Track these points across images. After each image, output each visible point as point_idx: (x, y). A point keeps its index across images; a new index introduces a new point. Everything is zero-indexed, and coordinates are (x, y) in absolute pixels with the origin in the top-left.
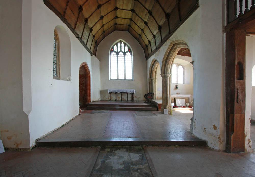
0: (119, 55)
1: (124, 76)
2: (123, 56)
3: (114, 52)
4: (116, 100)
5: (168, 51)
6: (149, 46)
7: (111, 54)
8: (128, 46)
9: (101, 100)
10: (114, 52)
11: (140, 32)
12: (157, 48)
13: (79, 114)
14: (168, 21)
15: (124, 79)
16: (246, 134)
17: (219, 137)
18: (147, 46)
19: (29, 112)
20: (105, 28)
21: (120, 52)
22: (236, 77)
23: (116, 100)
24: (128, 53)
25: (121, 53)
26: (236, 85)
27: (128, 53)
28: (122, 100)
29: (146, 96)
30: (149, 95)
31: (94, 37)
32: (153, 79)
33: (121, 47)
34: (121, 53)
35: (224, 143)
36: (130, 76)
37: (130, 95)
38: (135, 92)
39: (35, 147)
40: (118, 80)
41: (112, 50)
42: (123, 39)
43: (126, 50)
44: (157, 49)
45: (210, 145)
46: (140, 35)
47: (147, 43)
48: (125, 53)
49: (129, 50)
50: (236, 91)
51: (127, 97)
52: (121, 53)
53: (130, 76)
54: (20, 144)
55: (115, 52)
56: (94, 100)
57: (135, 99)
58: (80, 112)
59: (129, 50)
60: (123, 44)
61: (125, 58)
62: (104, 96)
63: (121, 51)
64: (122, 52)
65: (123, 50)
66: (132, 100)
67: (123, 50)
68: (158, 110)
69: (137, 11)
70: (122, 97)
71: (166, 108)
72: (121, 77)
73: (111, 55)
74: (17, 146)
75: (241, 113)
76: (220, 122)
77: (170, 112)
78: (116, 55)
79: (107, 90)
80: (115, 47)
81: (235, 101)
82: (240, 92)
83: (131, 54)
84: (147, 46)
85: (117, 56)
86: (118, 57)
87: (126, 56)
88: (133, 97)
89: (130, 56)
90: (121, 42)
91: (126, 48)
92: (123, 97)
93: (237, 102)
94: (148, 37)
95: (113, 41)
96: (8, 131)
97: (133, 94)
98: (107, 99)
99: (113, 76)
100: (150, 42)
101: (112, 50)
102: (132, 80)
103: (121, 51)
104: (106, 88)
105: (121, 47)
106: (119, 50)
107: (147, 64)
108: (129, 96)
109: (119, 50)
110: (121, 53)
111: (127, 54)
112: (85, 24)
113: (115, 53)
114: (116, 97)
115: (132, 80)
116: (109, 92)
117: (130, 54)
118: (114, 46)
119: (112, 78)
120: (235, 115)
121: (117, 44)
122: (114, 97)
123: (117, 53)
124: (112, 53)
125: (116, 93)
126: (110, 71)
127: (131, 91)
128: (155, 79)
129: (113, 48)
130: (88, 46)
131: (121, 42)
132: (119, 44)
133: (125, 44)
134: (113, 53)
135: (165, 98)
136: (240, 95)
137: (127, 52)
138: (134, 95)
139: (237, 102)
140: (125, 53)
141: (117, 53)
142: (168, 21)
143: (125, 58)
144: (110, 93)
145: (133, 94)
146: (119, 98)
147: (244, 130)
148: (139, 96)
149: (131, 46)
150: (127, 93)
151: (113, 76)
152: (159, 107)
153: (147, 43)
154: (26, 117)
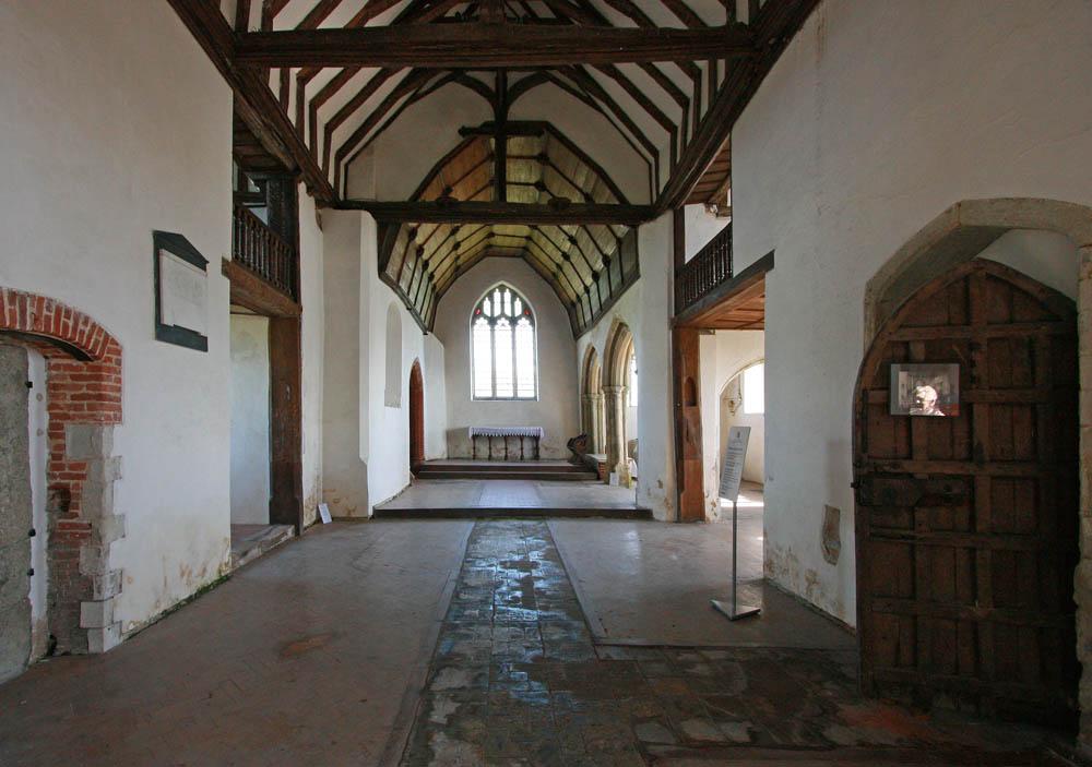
0: (496, 327)
1: (511, 387)
2: (509, 328)
3: (482, 318)
4: (490, 456)
5: (613, 335)
6: (579, 306)
7: (473, 323)
8: (521, 300)
9: (448, 458)
10: (482, 318)
11: (554, 268)
12: (626, 278)
13: (410, 485)
14: (608, 270)
15: (511, 395)
16: (706, 494)
17: (666, 500)
18: (573, 304)
19: (367, 459)
20: (460, 262)
21: (499, 317)
22: (684, 400)
23: (490, 458)
24: (524, 319)
25: (503, 320)
26: (684, 412)
27: (524, 319)
28: (506, 456)
29: (571, 444)
30: (581, 443)
31: (431, 277)
32: (617, 388)
33: (503, 303)
34: (503, 320)
35: (675, 509)
36: (527, 389)
37: (530, 443)
38: (542, 435)
39: (373, 517)
40: (494, 398)
41: (479, 313)
42: (507, 281)
43: (518, 311)
44: (595, 320)
45: (655, 516)
46: (554, 274)
47: (574, 298)
48: (513, 321)
49: (527, 312)
50: (685, 426)
51: (522, 449)
52: (503, 319)
53: (527, 389)
54: (354, 511)
55: (486, 317)
56: (432, 458)
57: (543, 453)
58: (411, 479)
59: (527, 312)
60: (508, 295)
61: (513, 336)
62: (457, 446)
63: (503, 314)
64: (507, 318)
65: (508, 312)
66: (536, 457)
67: (508, 312)
68: (599, 479)
69: (553, 155)
70: (506, 449)
71: (614, 471)
72: (505, 391)
73: (476, 327)
74: (349, 512)
75: (695, 459)
76: (667, 474)
77: (624, 482)
78: (489, 327)
79: (467, 430)
80: (487, 304)
81: (685, 440)
82: (691, 425)
83: (532, 323)
84: (573, 304)
85: (493, 330)
86: (496, 332)
87: (517, 328)
88: (536, 449)
89: (531, 328)
90: (502, 289)
91: (518, 304)
92: (510, 448)
93: (688, 440)
94: (577, 281)
95: (481, 288)
96: (334, 491)
97: (536, 438)
98: (466, 455)
99: (481, 387)
100: (587, 290)
101: (479, 313)
102: (536, 398)
103: (503, 314)
104: (461, 424)
105: (503, 303)
106: (497, 312)
107: (576, 349)
108: (528, 445)
109: (497, 312)
110: (503, 319)
111: (519, 322)
112: (410, 241)
113: (486, 321)
114: (490, 448)
115: (535, 398)
116: (470, 435)
117: (528, 322)
118: (484, 299)
119: (478, 394)
120: (686, 462)
121: (491, 295)
122: (483, 450)
123: (492, 321)
124: (477, 321)
125: (490, 438)
126: (474, 373)
127: (531, 430)
128: (623, 388)
129: (480, 307)
130: (412, 298)
131: (502, 289)
132: (497, 295)
133: (514, 296)
134: (481, 322)
135: (613, 448)
136: (693, 430)
137: (520, 317)
138: (540, 442)
139: (688, 440)
140: (513, 321)
141: (492, 321)
142: (608, 270)
143: (513, 336)
144: (475, 437)
145: (536, 438)
146: (499, 451)
147: (701, 487)
148: (555, 446)
149: (530, 300)
150: (522, 438)
151: (481, 387)
152: (600, 470)
153: (574, 298)
154: (363, 467)
